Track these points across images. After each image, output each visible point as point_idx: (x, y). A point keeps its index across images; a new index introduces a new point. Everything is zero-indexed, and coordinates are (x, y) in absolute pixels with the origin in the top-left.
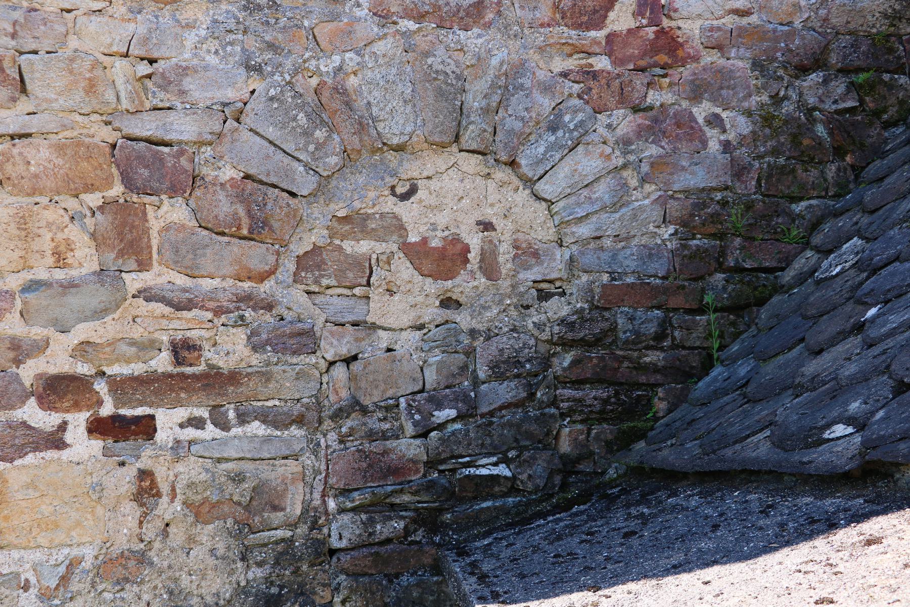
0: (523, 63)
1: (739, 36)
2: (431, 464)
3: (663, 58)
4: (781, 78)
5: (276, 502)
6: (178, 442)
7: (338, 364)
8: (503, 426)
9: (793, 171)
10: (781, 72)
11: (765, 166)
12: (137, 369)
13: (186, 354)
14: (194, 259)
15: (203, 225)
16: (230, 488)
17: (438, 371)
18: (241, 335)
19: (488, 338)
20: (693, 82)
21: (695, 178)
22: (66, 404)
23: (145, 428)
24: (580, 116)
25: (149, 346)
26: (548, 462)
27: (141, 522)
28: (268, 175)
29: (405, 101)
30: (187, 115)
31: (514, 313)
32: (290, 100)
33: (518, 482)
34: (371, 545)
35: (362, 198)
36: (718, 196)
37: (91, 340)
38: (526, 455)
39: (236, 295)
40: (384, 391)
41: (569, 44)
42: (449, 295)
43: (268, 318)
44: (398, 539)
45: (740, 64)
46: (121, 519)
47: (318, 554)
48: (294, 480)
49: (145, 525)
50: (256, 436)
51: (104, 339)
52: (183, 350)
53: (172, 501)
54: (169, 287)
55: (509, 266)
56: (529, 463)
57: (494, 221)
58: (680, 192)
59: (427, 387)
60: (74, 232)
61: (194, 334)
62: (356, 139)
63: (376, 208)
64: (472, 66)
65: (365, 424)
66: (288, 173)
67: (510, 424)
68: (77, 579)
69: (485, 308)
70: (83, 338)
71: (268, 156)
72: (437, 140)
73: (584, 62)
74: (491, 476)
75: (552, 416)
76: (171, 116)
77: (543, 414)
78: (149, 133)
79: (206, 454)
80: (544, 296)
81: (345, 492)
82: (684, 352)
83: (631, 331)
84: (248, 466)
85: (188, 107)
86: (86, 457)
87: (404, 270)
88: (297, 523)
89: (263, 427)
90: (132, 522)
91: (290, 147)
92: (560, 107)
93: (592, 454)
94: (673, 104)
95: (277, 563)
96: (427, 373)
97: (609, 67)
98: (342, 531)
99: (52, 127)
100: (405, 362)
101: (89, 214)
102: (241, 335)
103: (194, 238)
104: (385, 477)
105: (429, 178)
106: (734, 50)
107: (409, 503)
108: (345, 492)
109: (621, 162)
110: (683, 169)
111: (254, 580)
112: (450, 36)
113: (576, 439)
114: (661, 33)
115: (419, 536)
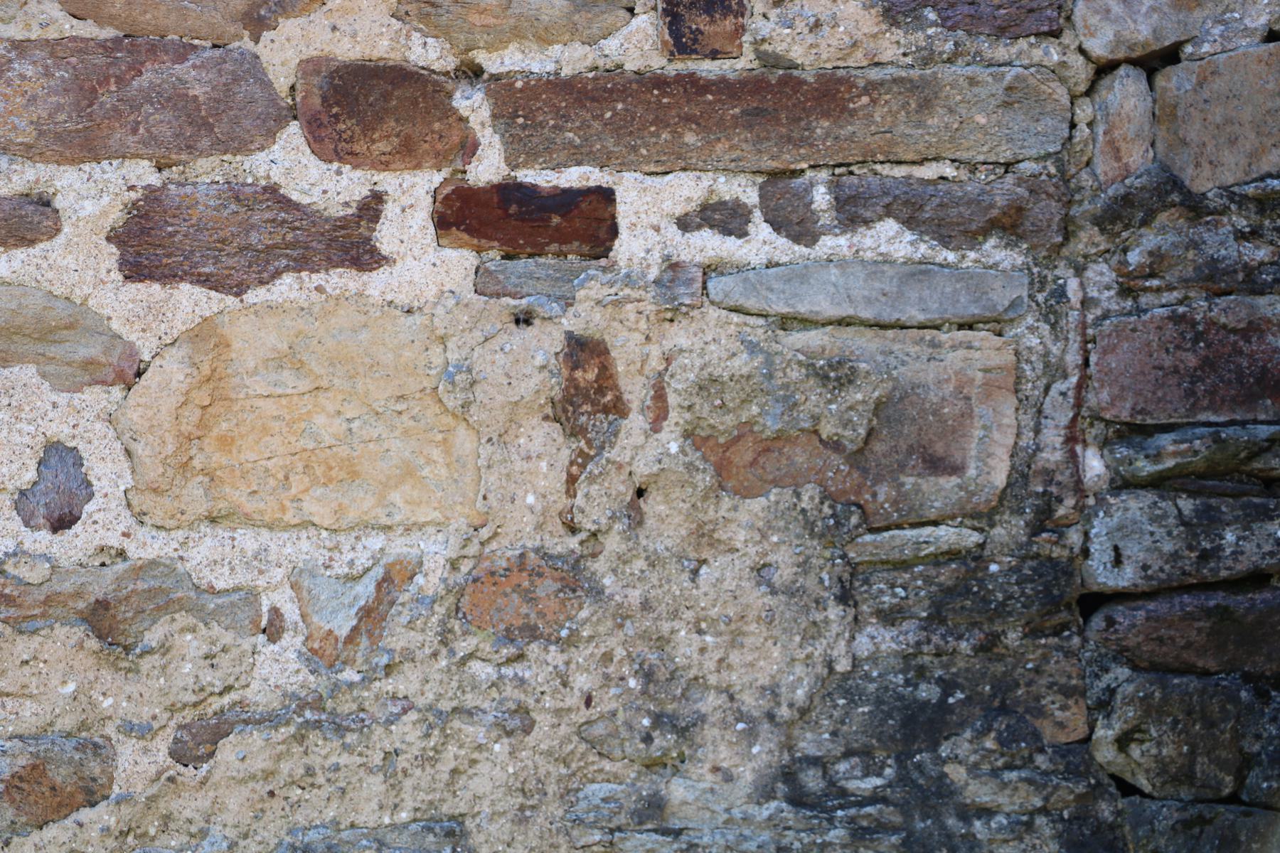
5: (939, 449)
6: (673, 266)
7: (1122, 71)
12: (570, 58)
16: (813, 398)
22: (382, 146)
27: (572, 480)
40: (1254, 155)
46: (519, 465)
47: (1053, 603)
48: (989, 390)
49: (582, 488)
50: (887, 260)
53: (656, 426)
65: (1195, 245)
68: (404, 619)
79: (751, 303)
81: (1133, 432)
84: (862, 343)
88: (993, 511)
89: (909, 236)
90: (549, 476)
95: (936, 617)
98: (1123, 542)
104: (1249, 399)
108: (1133, 432)
111: (873, 658)
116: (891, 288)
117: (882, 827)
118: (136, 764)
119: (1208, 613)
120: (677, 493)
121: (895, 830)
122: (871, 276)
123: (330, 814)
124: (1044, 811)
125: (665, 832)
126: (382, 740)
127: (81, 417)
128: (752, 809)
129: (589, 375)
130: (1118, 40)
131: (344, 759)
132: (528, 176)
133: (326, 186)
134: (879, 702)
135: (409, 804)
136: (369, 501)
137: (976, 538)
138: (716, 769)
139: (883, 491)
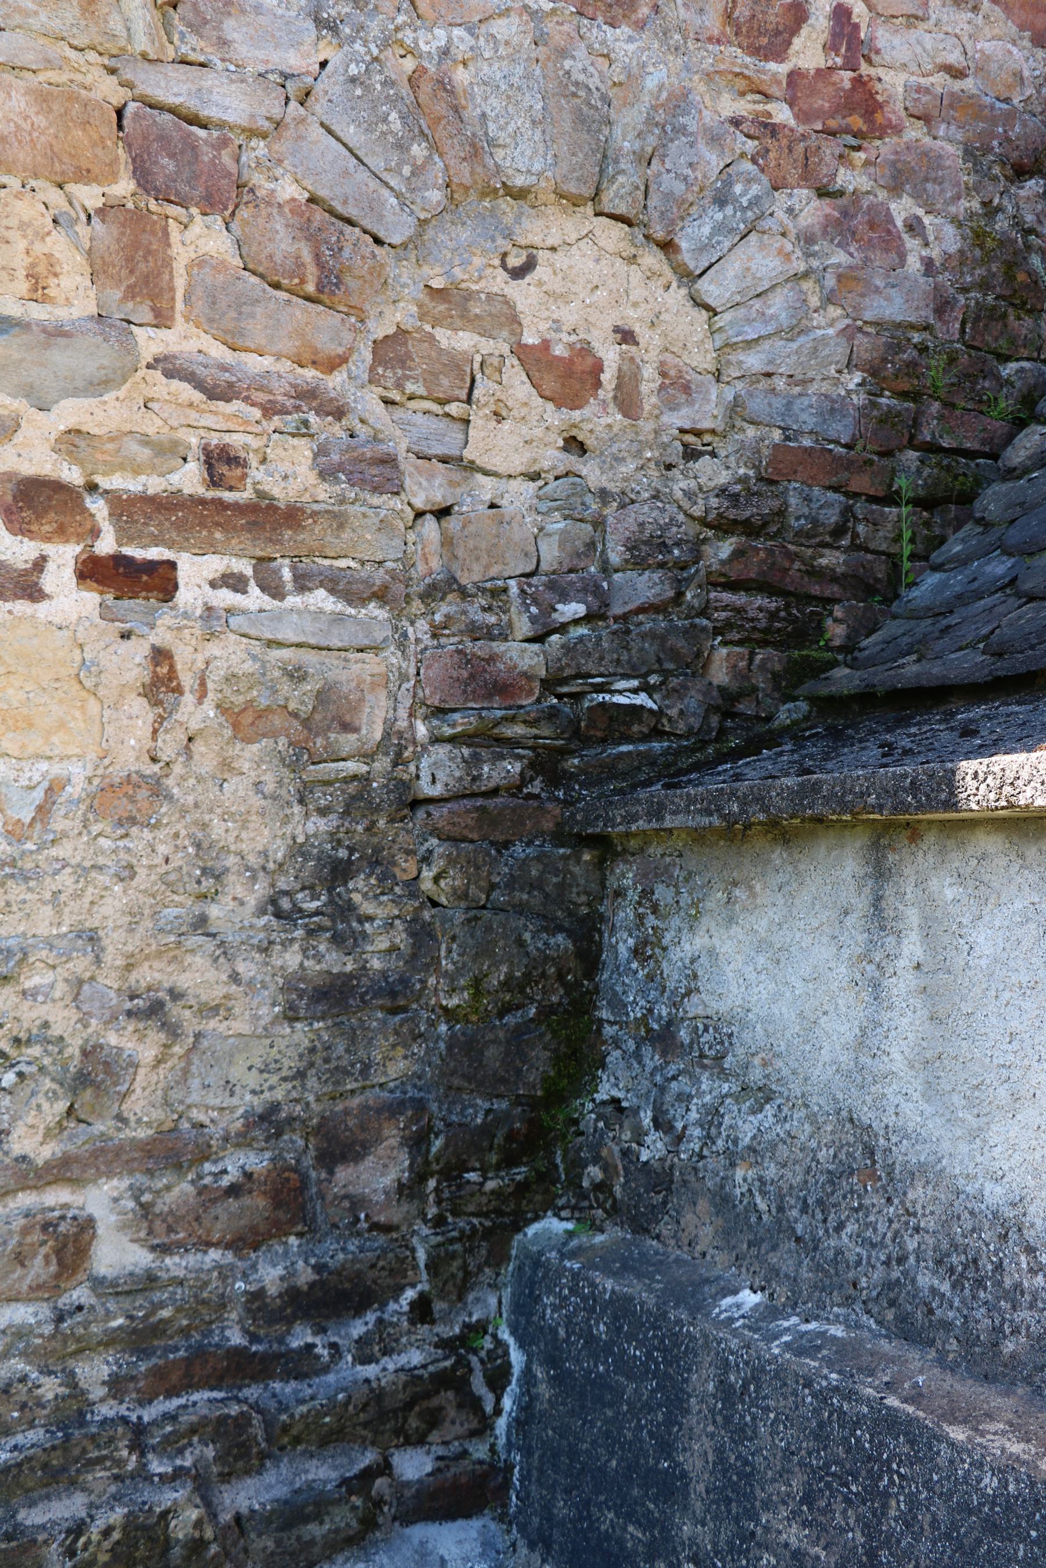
0: (686, 94)
1: (951, 106)
2: (549, 684)
3: (857, 122)
4: (995, 179)
5: (347, 718)
6: (209, 609)
7: (428, 516)
8: (643, 636)
9: (1004, 316)
10: (996, 170)
11: (973, 303)
12: (154, 485)
13: (224, 469)
14: (238, 320)
15: (250, 266)
16: (285, 687)
17: (561, 545)
18: (304, 449)
19: (622, 506)
20: (894, 163)
21: (892, 306)
22: (47, 528)
23: (160, 580)
24: (755, 189)
25: (170, 451)
26: (705, 694)
27: (155, 732)
28: (345, 202)
29: (533, 122)
30: (232, 81)
31: (653, 472)
32: (378, 87)
33: (665, 721)
34: (473, 795)
35: (465, 263)
36: (916, 337)
37: (84, 429)
38: (674, 682)
39: (294, 386)
40: (487, 567)
41: (745, 77)
42: (574, 432)
43: (337, 430)
44: (508, 789)
45: (950, 148)
46: (126, 722)
47: (402, 804)
48: (373, 686)
49: (161, 736)
50: (321, 611)
51: (106, 429)
52: (220, 462)
53: (200, 700)
54: (201, 358)
55: (654, 400)
56: (678, 693)
57: (637, 329)
58: (871, 323)
59: (544, 566)
60: (58, 244)
61: (236, 440)
62: (465, 168)
63: (482, 284)
64: (621, 84)
65: (464, 612)
66: (374, 206)
67: (652, 635)
68: (62, 812)
69: (619, 460)
70: (71, 422)
71: (346, 173)
72: (573, 190)
73: (760, 107)
74: (633, 707)
75: (704, 629)
76: (209, 79)
77: (693, 626)
78: (178, 101)
79: (253, 632)
80: (691, 454)
81: (440, 712)
82: (869, 556)
83: (806, 518)
84: (309, 658)
85: (232, 68)
86: (74, 617)
87: (517, 385)
88: (374, 753)
89: (332, 599)
90: (143, 726)
91: (377, 163)
92: (729, 170)
93: (755, 689)
94: (868, 193)
95: (346, 813)
96: (543, 547)
97: (792, 123)
98: (436, 771)
99: (28, 58)
100: (514, 525)
101: (83, 217)
102: (304, 449)
103: (240, 285)
104: (489, 696)
105: (553, 249)
106: (943, 126)
107: (523, 737)
108: (440, 712)
109: (802, 267)
110: (877, 290)
111: (315, 835)
112: (595, 31)
113: (735, 666)
114: (859, 82)
115: (536, 787)
116: (324, 627)
117: (321, 928)
119: (477, 809)
120: (213, 740)
121: (328, 930)
122: (314, 620)
123: (21, 929)
124: (398, 917)
125: (208, 935)
126: (50, 885)
128: (255, 921)
129: (163, 670)
130: (427, 501)
131: (29, 896)
132: (128, 551)
134: (319, 859)
135: (67, 922)
136: (40, 742)
137: (366, 768)
138: (235, 899)
139: (320, 741)
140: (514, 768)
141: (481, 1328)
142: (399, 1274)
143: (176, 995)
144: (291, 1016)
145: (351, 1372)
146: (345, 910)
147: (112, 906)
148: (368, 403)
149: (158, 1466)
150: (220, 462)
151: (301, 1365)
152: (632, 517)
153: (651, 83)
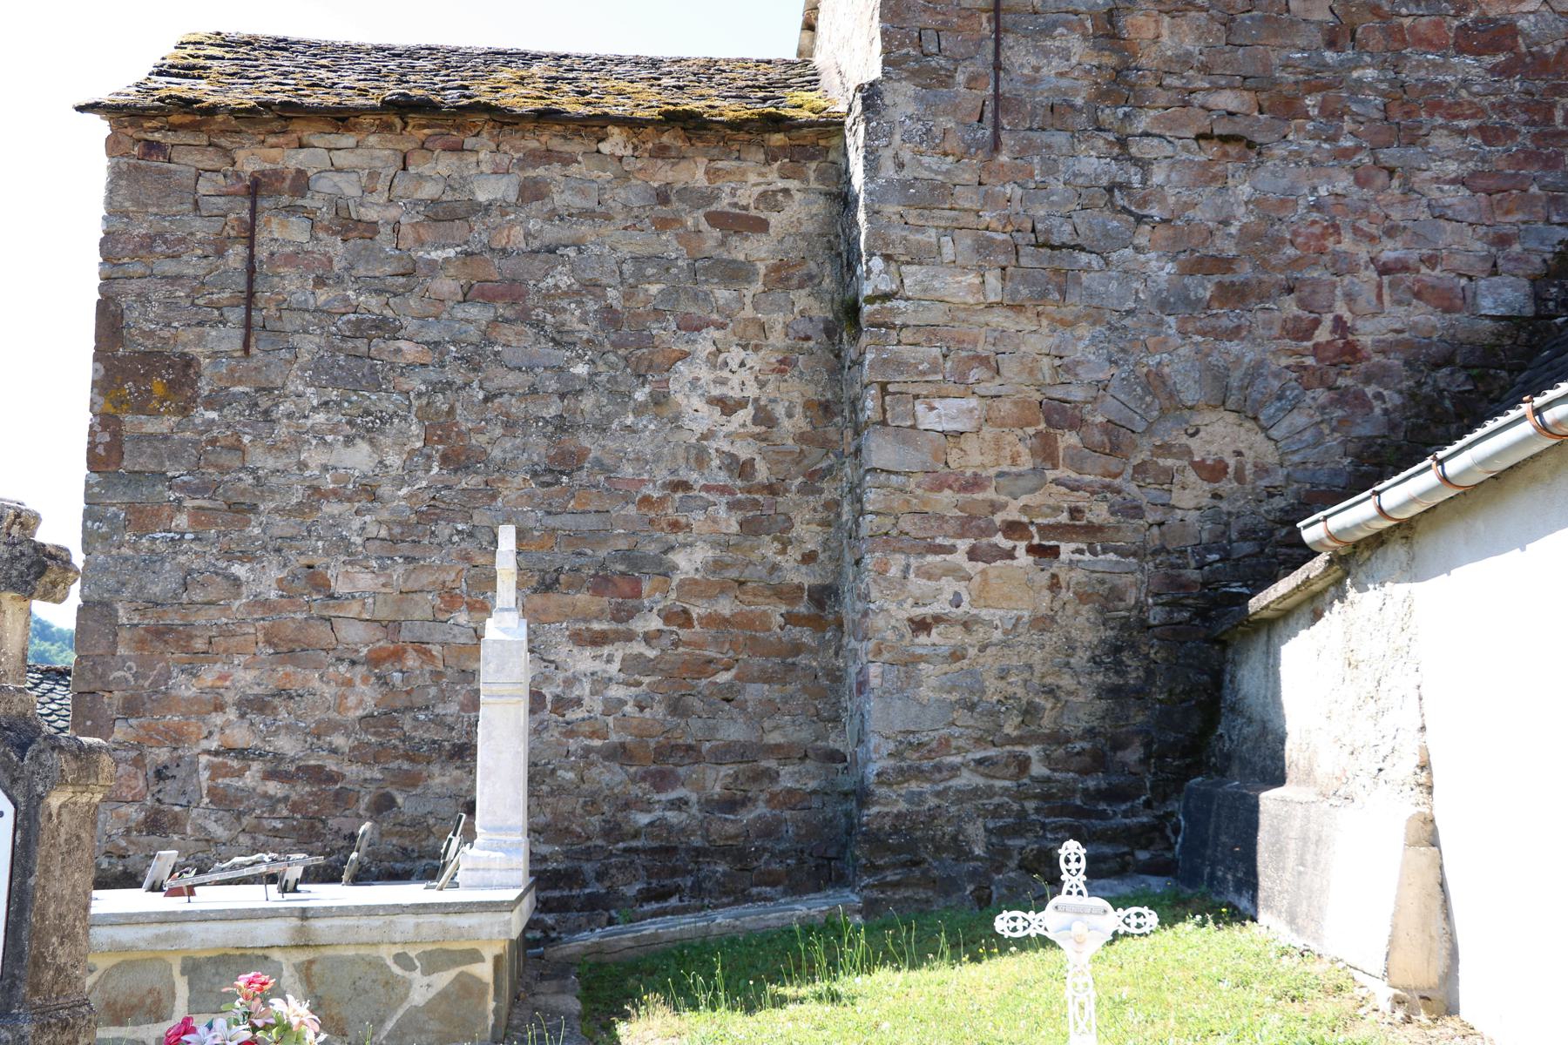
2: (1204, 585)
3: (1347, 358)
12: (1052, 521)
21: (1365, 430)
23: (1054, 552)
25: (1057, 510)
43: (1119, 498)
52: (1075, 512)
60: (1021, 447)
66: (1131, 420)
76: (1071, 388)
80: (1271, 496)
81: (1157, 595)
84: (1107, 576)
87: (1191, 476)
91: (1132, 406)
98: (1156, 616)
102: (1105, 506)
108: (1157, 595)
118: (972, 652)
127: (960, 587)
133: (1006, 544)
140: (1187, 615)
141: (1172, 814)
142: (1139, 791)
143: (1059, 687)
144: (1099, 697)
145: (1120, 820)
146: (1121, 663)
147: (1038, 655)
148: (1133, 487)
149: (1049, 836)
150: (1075, 512)
151: (1102, 815)
152: (1241, 522)
153: (1246, 360)
